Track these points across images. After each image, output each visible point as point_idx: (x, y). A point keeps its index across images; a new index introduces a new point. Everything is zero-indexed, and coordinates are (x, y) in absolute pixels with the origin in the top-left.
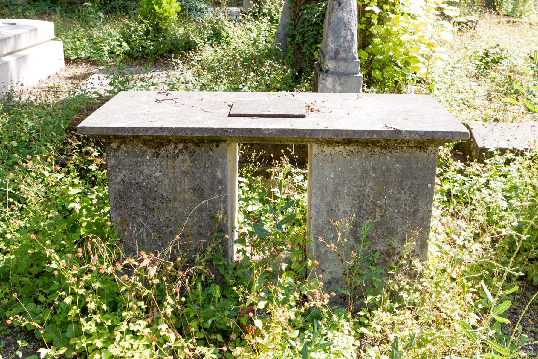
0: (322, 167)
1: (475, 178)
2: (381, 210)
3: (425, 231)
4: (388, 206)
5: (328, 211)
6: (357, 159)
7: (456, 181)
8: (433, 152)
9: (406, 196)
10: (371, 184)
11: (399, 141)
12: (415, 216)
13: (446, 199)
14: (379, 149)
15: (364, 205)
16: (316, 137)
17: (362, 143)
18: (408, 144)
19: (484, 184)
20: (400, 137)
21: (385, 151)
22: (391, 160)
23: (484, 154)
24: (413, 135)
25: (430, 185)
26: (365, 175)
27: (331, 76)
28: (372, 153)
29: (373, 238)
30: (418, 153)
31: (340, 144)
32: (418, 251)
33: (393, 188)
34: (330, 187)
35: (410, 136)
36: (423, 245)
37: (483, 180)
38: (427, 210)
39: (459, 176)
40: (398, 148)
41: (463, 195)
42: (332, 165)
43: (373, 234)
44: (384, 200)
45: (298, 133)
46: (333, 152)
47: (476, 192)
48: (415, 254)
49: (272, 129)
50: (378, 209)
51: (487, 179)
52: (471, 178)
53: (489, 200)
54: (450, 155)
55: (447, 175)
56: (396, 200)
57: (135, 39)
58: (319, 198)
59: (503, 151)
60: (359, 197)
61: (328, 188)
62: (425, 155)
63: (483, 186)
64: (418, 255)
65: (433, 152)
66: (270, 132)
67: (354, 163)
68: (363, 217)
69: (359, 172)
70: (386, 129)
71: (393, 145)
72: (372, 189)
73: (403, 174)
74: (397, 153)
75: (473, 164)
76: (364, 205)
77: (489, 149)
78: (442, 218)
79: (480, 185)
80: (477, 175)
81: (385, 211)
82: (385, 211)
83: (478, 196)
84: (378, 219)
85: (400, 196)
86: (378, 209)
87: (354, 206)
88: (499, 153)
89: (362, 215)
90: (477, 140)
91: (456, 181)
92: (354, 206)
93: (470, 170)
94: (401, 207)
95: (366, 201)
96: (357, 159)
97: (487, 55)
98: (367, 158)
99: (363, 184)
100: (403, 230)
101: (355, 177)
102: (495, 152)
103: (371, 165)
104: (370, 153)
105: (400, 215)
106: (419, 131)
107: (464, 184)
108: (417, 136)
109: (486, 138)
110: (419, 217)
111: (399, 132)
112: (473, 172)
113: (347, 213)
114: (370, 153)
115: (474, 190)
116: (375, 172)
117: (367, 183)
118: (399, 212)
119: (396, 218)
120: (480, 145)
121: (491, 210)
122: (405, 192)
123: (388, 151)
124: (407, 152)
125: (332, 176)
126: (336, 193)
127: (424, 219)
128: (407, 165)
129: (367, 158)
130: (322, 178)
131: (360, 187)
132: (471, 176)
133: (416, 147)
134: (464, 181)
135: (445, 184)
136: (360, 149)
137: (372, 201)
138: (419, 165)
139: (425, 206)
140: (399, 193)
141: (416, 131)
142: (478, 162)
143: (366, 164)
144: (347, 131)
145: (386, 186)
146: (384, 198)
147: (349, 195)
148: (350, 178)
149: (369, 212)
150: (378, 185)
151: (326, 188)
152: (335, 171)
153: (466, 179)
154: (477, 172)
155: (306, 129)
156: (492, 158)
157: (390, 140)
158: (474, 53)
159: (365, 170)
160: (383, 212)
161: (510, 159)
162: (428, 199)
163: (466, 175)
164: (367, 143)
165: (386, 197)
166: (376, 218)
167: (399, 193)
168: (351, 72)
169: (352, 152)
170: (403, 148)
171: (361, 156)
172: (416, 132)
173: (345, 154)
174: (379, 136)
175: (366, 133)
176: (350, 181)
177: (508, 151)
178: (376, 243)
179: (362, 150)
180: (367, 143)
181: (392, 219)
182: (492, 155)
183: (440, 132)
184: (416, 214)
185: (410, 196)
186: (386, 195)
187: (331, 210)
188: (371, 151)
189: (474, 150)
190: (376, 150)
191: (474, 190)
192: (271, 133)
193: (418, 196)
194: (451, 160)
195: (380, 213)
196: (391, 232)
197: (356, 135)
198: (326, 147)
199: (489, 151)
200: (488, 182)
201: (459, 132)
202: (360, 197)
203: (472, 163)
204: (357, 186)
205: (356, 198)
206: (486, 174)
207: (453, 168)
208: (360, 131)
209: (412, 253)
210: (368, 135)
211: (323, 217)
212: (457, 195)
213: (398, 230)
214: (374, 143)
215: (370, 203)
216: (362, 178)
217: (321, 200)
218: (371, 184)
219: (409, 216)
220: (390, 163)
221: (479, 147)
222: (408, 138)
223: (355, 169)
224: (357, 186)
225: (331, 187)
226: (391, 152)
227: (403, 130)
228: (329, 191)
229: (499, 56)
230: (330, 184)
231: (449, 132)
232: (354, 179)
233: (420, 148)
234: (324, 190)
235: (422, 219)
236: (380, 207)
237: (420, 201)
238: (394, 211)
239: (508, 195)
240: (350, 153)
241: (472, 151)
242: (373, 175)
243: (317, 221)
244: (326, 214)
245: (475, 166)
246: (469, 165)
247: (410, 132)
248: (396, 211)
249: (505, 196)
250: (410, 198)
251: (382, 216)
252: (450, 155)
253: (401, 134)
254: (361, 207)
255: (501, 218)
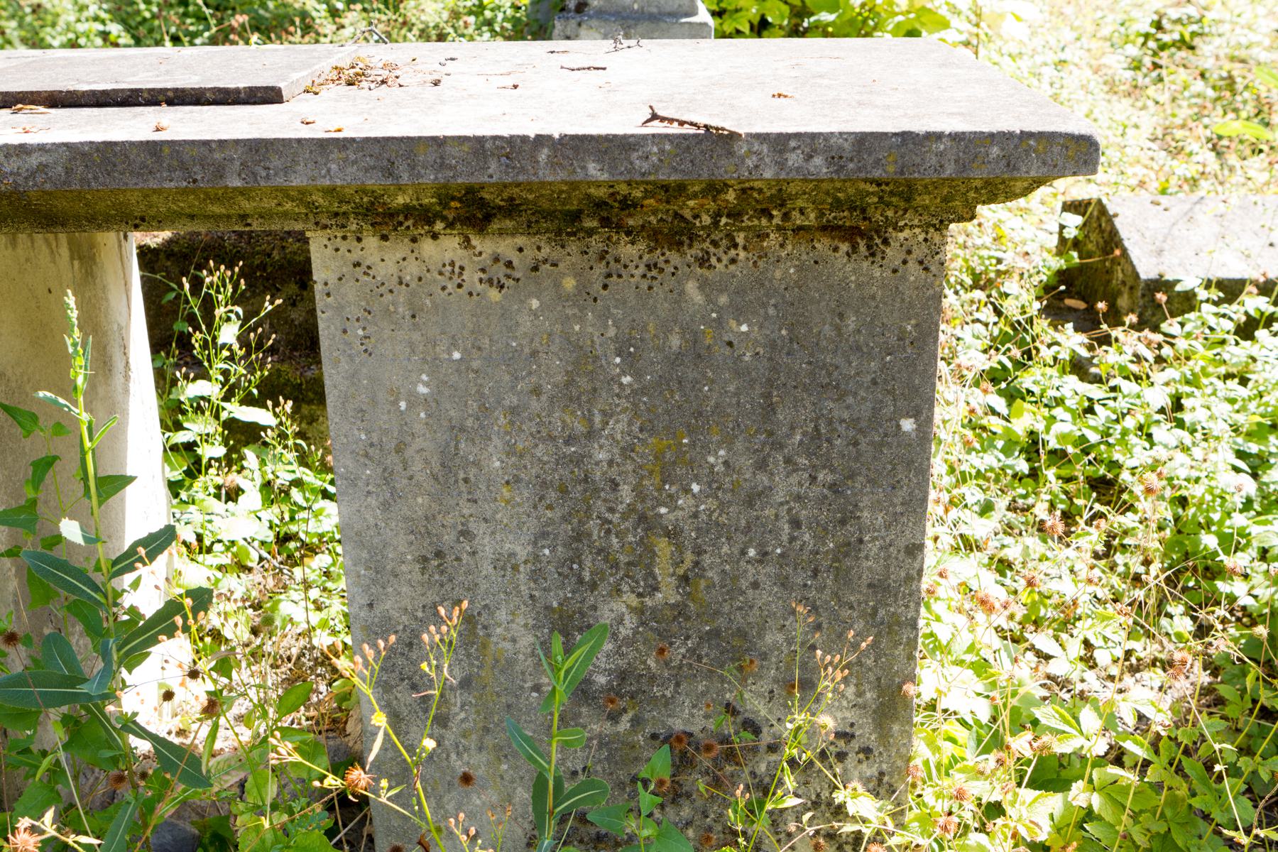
0: (369, 345)
1: (1128, 387)
2: (680, 548)
3: (897, 644)
4: (712, 529)
5: (425, 559)
6: (535, 304)
7: (1059, 402)
8: (918, 253)
9: (794, 479)
10: (618, 426)
11: (731, 196)
12: (843, 577)
13: (1023, 466)
14: (642, 245)
15: (593, 525)
16: (279, 181)
17: (549, 215)
18: (786, 217)
19: (1162, 411)
20: (725, 170)
21: (674, 257)
22: (709, 300)
23: (1161, 297)
24: (794, 159)
25: (908, 425)
26: (583, 382)
27: (594, 23)
28: (614, 270)
29: (652, 678)
30: (841, 262)
31: (439, 226)
32: (866, 734)
33: (728, 441)
34: (419, 443)
35: (781, 165)
36: (890, 705)
37: (1158, 397)
38: (902, 543)
39: (1072, 381)
40: (740, 238)
41: (1086, 452)
42: (416, 336)
43: (651, 662)
44: (686, 504)
45: (183, 167)
46: (412, 269)
47: (1133, 439)
48: (855, 745)
49: (42, 148)
50: (663, 547)
51: (1171, 390)
52: (1113, 389)
53: (1183, 473)
54: (1037, 305)
55: (1026, 380)
56: (750, 502)
57: (147, 15)
58: (372, 501)
59: (1230, 290)
60: (563, 490)
61: (409, 452)
62: (877, 273)
63: (1160, 417)
64: (867, 751)
65: (918, 253)
66: (34, 160)
67: (526, 323)
68: (593, 586)
69: (555, 366)
70: (657, 128)
71: (706, 220)
72: (628, 451)
73: (774, 369)
74: (735, 265)
75: (1121, 336)
76: (593, 525)
77: (1179, 281)
78: (1008, 540)
79: (1148, 416)
80: (1137, 378)
81: (699, 552)
82: (699, 552)
83: (1139, 454)
84: (668, 594)
85: (763, 479)
86: (663, 547)
87: (544, 535)
88: (1215, 294)
89: (587, 576)
90: (1136, 254)
91: (1059, 402)
92: (544, 535)
93: (1109, 358)
94: (775, 532)
95: (600, 507)
96: (535, 304)
97: (1159, 26)
98: (585, 296)
99: (580, 428)
100: (790, 641)
101: (537, 391)
102: (1202, 294)
103: (612, 332)
104: (600, 269)
105: (770, 569)
106: (827, 137)
107: (1090, 410)
108: (818, 160)
109: (1166, 246)
110: (865, 579)
111: (719, 141)
112: (1122, 368)
113: (515, 568)
114: (600, 269)
115: (1125, 433)
116: (631, 364)
117: (598, 419)
118: (764, 555)
119: (755, 585)
120: (1147, 269)
121: (1191, 511)
122: (788, 461)
123: (696, 251)
124: (786, 262)
125: (422, 389)
126: (450, 471)
127: (887, 589)
128: (790, 331)
129: (585, 296)
130: (374, 402)
131: (567, 442)
132: (1112, 383)
133: (827, 229)
134: (1090, 400)
135: (1019, 414)
136: (546, 250)
137: (631, 509)
138: (851, 322)
139: (888, 527)
140: (761, 465)
141: (813, 136)
142: (1138, 327)
143: (587, 327)
144: (438, 142)
145: (691, 431)
146: (687, 490)
147: (518, 480)
148: (511, 400)
149: (623, 559)
150: (653, 431)
151: (398, 450)
152: (433, 365)
153: (1096, 392)
154: (1134, 368)
155: (222, 143)
156: (1192, 316)
157: (681, 188)
158: (1122, 24)
159: (583, 359)
160: (689, 557)
161: (1257, 316)
162: (902, 493)
163: (1097, 380)
164: (576, 216)
165: (695, 488)
166: (656, 589)
167: (761, 465)
168: (668, 9)
169: (509, 264)
170: (763, 236)
171: (557, 285)
172: (811, 142)
173: (472, 277)
174: (612, 169)
175: (543, 155)
176: (514, 411)
177: (1249, 288)
178: (667, 702)
179: (557, 254)
180: (576, 216)
181: (734, 592)
182: (1187, 302)
183: (938, 136)
184: (848, 562)
185: (813, 479)
186: (697, 479)
187: (439, 554)
188: (602, 256)
189: (1126, 290)
190: (628, 250)
191: (1125, 433)
192: (43, 167)
193: (852, 476)
194: (1042, 325)
195: (677, 565)
196: (735, 649)
197: (493, 166)
198: (371, 242)
199: (1178, 288)
200: (1178, 405)
201: (1041, 136)
202: (571, 489)
203: (1116, 332)
204: (552, 438)
205: (552, 495)
206: (1171, 373)
207: (1046, 354)
208: (511, 140)
209: (841, 743)
210: (553, 164)
211: (405, 589)
212: (1064, 454)
213: (769, 639)
214: (611, 212)
215: (624, 517)
216: (569, 396)
217: (386, 506)
218: (618, 426)
219: (816, 573)
220: (705, 320)
221: (1143, 276)
222: (768, 174)
223: (534, 354)
224: (552, 438)
225: (424, 445)
226: (703, 261)
227: (742, 131)
228: (417, 466)
229: (1195, 27)
230: (418, 428)
231: (992, 135)
232: (535, 405)
233: (850, 234)
234: (392, 460)
235: (880, 588)
236: (673, 534)
237: (865, 501)
238: (743, 552)
239: (1253, 448)
240: (499, 271)
241: (1119, 293)
242: (626, 380)
243: (378, 609)
244: (417, 576)
245: (1129, 343)
246: (1106, 340)
247: (780, 143)
248: (752, 552)
249: (1241, 454)
250: (816, 491)
251: (685, 579)
252: (1037, 305)
253: (731, 153)
254: (580, 535)
255: (1232, 543)
